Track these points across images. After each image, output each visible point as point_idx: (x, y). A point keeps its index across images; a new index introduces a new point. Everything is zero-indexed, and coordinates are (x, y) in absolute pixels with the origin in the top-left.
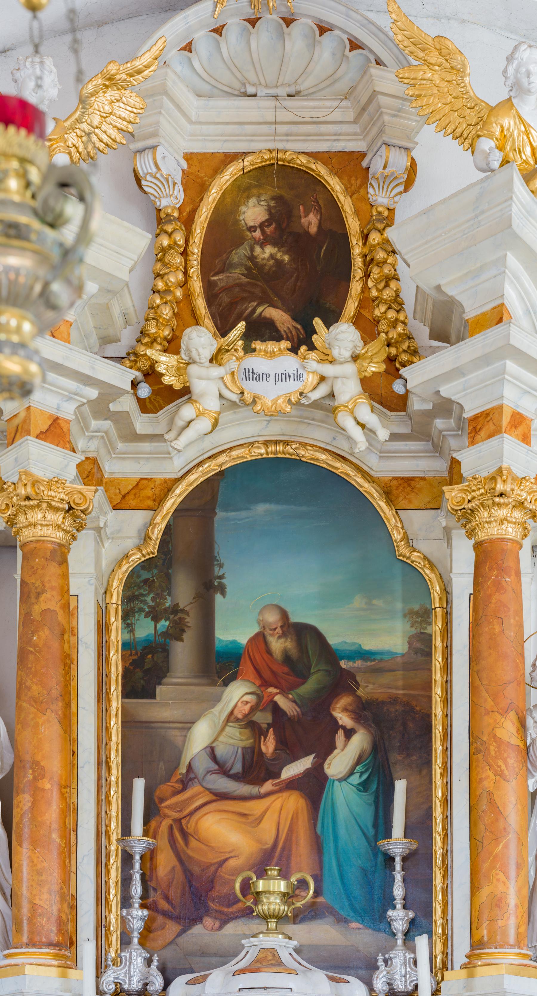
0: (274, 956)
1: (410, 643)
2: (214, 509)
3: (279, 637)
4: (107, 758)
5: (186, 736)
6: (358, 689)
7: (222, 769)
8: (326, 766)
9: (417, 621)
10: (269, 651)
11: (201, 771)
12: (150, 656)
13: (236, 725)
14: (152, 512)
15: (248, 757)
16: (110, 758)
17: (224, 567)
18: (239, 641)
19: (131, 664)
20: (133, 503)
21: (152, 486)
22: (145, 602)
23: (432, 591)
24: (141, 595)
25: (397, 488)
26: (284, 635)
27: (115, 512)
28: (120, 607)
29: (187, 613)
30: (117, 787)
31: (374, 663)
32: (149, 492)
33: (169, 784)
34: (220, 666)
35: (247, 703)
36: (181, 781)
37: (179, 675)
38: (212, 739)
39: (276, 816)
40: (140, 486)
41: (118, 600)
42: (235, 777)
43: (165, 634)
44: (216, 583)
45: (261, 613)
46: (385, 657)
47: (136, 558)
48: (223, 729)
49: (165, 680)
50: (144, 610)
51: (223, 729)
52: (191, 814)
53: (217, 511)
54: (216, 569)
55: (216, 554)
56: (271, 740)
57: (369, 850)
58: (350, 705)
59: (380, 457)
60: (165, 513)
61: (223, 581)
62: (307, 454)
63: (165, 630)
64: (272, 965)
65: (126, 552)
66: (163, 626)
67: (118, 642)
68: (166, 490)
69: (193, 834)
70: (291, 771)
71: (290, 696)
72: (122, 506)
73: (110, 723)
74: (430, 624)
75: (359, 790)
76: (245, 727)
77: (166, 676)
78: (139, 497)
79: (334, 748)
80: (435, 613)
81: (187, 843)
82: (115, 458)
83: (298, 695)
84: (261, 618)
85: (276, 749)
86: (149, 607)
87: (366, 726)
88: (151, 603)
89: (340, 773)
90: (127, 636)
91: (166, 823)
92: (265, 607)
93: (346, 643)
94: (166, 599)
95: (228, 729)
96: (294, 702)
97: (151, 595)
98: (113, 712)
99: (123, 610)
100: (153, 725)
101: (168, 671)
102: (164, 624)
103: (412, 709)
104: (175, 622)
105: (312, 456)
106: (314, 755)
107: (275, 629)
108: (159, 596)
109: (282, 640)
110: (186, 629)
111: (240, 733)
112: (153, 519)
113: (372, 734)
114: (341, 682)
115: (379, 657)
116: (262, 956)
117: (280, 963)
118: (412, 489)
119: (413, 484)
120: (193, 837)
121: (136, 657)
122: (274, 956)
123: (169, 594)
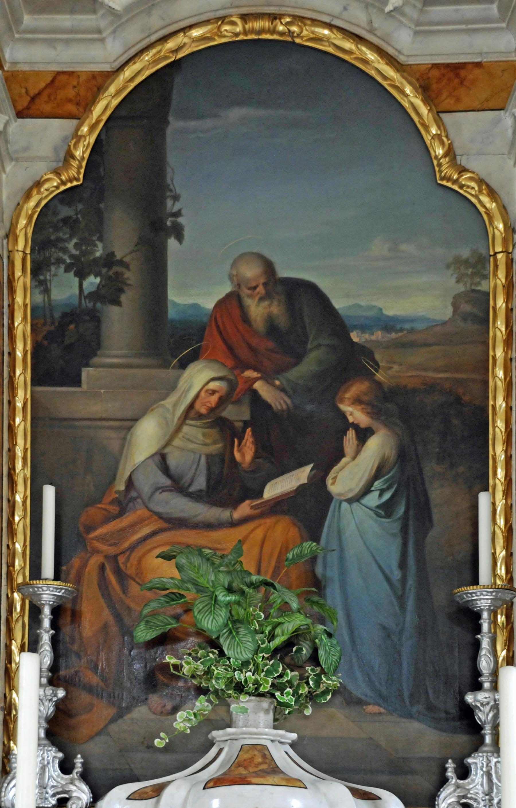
0: (264, 756)
1: (455, 306)
2: (166, 115)
3: (261, 299)
4: (9, 469)
5: (124, 439)
6: (377, 371)
7: (178, 486)
8: (329, 481)
9: (467, 274)
10: (246, 319)
11: (258, 319)
12: (72, 327)
13: (198, 423)
14: (75, 122)
15: (216, 469)
16: (14, 470)
17: (181, 200)
18: (202, 305)
19: (45, 337)
20: (47, 108)
21: (75, 83)
22: (65, 250)
23: (490, 230)
24: (59, 240)
25: (439, 81)
26: (267, 296)
27: (20, 121)
28: (29, 257)
29: (127, 266)
30: (25, 510)
31: (400, 334)
32: (71, 93)
33: (99, 506)
34: (174, 342)
35: (214, 392)
36: (117, 502)
37: (115, 352)
38: (163, 443)
39: (256, 551)
40: (57, 83)
41: (25, 246)
42: (196, 497)
43: (96, 296)
44: (169, 223)
45: (235, 264)
46: (419, 326)
47: (53, 186)
48: (178, 429)
49: (95, 360)
50: (63, 261)
51: (178, 429)
52: (132, 548)
53: (171, 119)
54: (169, 203)
55: (169, 181)
56: (248, 444)
57: (394, 600)
58: (365, 394)
59: (416, 33)
60: (94, 121)
61: (180, 220)
62: (304, 34)
63: (94, 289)
64: (263, 771)
65: (38, 179)
66: (92, 284)
67: (25, 306)
68: (95, 89)
69: (134, 576)
70: (275, 489)
71: (277, 383)
72: (31, 112)
73: (14, 421)
74: (486, 277)
75: (379, 515)
76: (211, 426)
77: (95, 355)
78: (55, 99)
79: (340, 454)
80: (495, 260)
81: (125, 590)
82: (19, 40)
83: (288, 380)
84: (235, 273)
85: (256, 456)
86: (71, 256)
87: (388, 425)
88: (74, 252)
89: (350, 490)
90: (39, 298)
91: (95, 561)
92: (242, 256)
93: (359, 306)
94: (96, 246)
95: (186, 429)
96: (283, 390)
97: (75, 241)
98: (19, 404)
99: (32, 262)
100: (77, 423)
101: (99, 346)
102: (92, 282)
103: (458, 400)
104: (110, 278)
105: (312, 36)
106: (311, 465)
107: (255, 288)
108: (85, 242)
109: (266, 303)
110: (126, 288)
111: (204, 435)
112: (78, 129)
113: (397, 434)
114: (351, 362)
115: (407, 326)
116: (246, 756)
117: (275, 770)
118: (462, 83)
119: (463, 73)
120: (134, 580)
121: (52, 328)
122: (264, 756)
123: (101, 239)
